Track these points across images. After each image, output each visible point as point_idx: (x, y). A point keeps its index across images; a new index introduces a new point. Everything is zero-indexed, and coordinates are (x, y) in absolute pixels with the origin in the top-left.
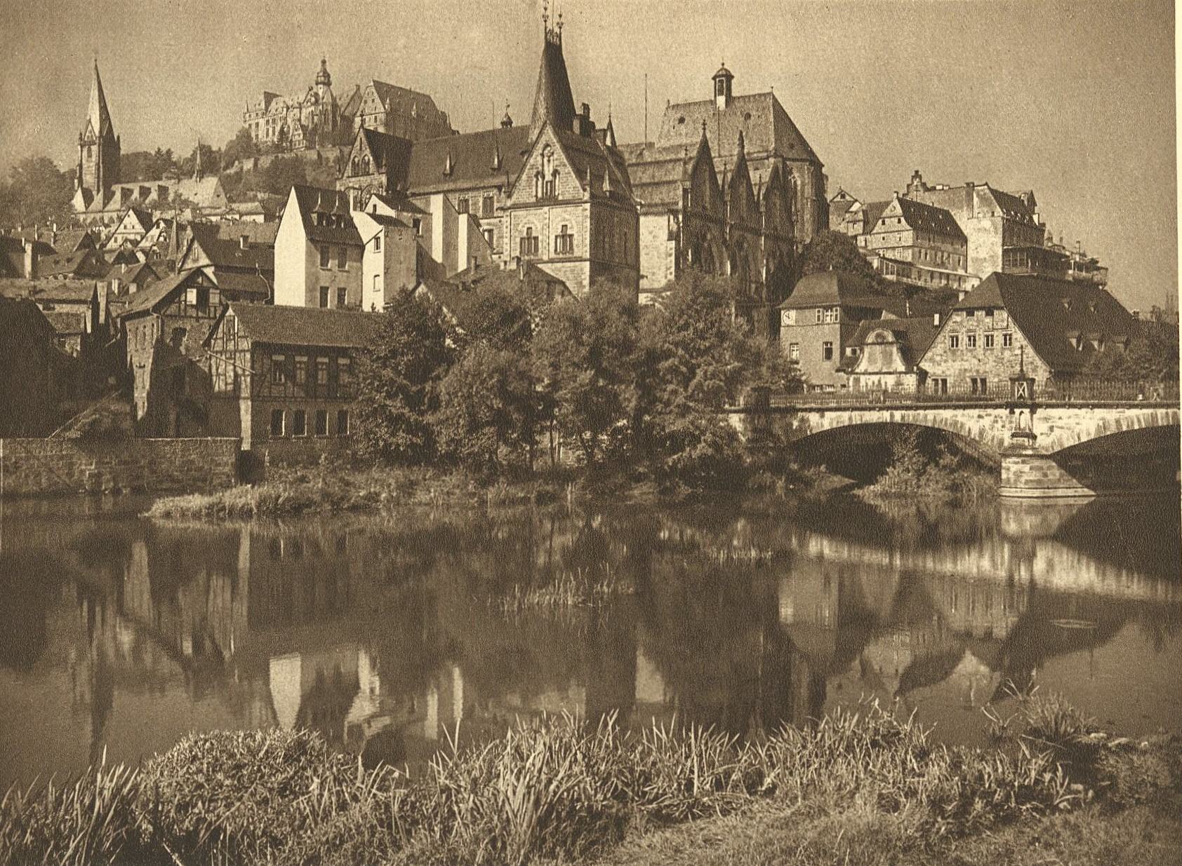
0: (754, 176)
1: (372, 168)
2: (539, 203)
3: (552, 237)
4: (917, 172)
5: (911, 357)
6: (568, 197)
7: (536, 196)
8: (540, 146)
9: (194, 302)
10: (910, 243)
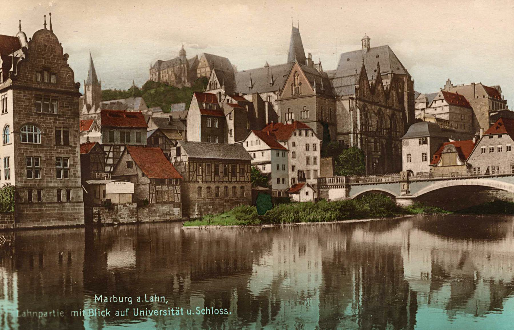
0: (384, 82)
1: (219, 85)
2: (293, 98)
3: (300, 112)
4: (449, 79)
5: (463, 158)
6: (306, 94)
7: (292, 94)
8: (293, 72)
9: (159, 139)
10: (448, 111)
